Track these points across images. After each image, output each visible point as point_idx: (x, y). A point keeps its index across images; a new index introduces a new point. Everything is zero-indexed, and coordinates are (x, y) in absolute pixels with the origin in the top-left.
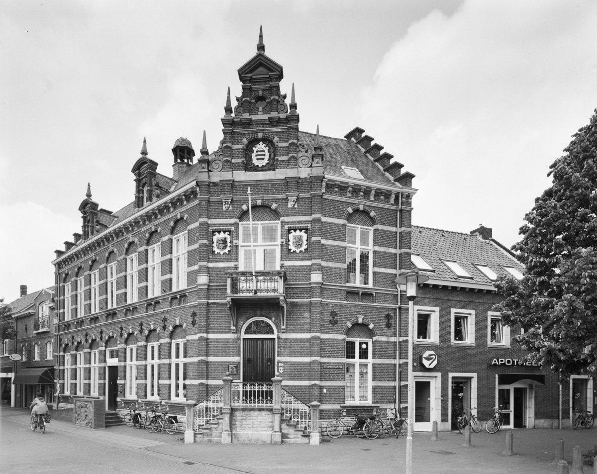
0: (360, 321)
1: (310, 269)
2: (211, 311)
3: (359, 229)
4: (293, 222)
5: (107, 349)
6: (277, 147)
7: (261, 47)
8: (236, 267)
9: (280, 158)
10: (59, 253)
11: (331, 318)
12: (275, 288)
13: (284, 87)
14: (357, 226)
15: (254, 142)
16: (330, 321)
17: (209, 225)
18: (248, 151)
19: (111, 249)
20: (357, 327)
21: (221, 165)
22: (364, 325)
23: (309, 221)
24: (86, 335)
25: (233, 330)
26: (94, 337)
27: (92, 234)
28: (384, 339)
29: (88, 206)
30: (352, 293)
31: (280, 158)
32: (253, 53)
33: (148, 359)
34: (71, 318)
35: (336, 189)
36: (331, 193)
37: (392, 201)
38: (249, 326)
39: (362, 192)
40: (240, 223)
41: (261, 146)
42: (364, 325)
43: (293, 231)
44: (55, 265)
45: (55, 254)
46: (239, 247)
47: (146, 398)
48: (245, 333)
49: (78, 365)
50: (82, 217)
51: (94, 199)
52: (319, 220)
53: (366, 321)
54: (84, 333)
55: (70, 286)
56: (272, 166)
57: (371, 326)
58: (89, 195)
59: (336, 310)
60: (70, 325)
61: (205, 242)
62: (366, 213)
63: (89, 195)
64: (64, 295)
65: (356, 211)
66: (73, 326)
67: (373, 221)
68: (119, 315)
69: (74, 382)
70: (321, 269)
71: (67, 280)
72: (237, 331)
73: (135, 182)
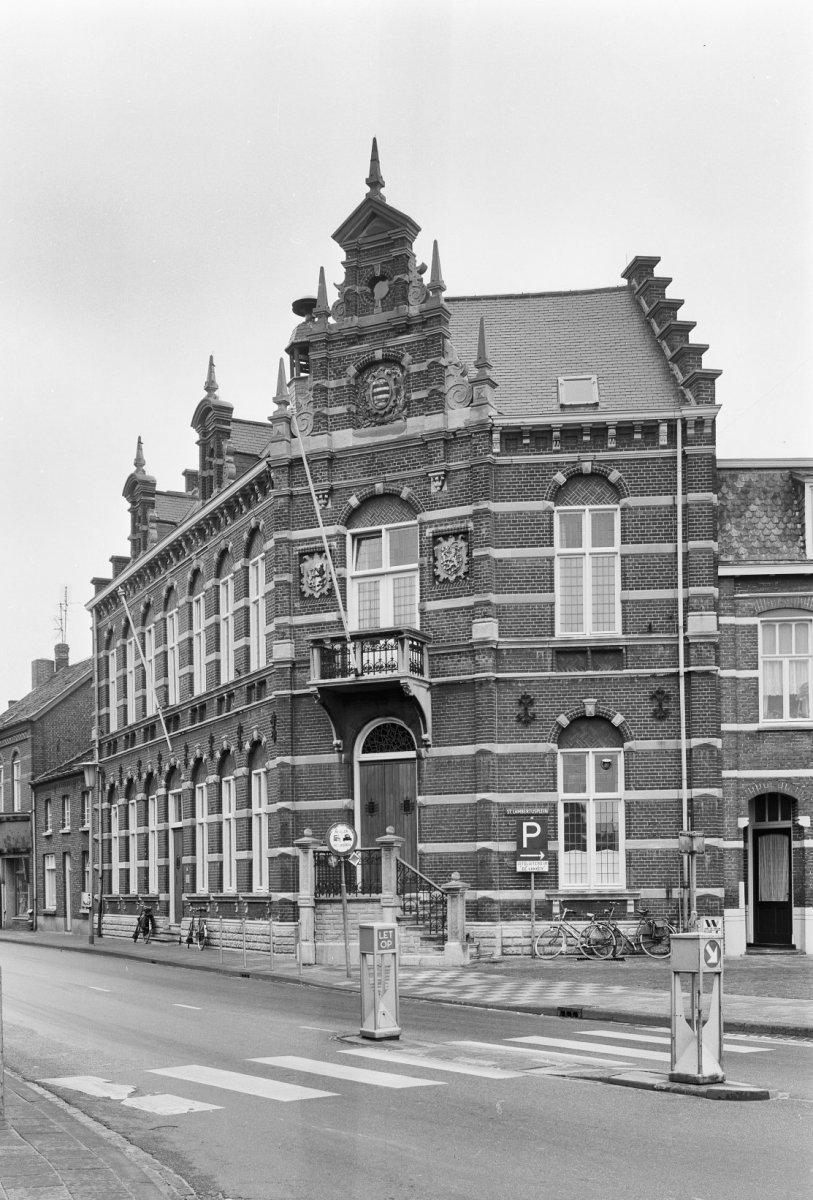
0: (590, 710)
1: (471, 612)
2: (300, 715)
3: (587, 513)
4: (440, 521)
5: (171, 792)
7: (375, 182)
8: (340, 624)
9: (414, 396)
10: (100, 584)
11: (520, 711)
12: (392, 663)
13: (421, 251)
14: (581, 507)
17: (290, 543)
18: (355, 391)
20: (583, 726)
21: (311, 421)
22: (602, 719)
23: (470, 516)
25: (338, 746)
27: (220, 483)
28: (652, 745)
30: (567, 652)
33: (223, 811)
36: (515, 449)
37: (663, 441)
38: (369, 739)
39: (586, 435)
42: (602, 719)
43: (441, 539)
44: (91, 611)
45: (93, 587)
46: (349, 581)
47: (222, 891)
48: (364, 752)
49: (255, 809)
50: (197, 443)
51: (223, 396)
52: (487, 512)
53: (604, 709)
54: (235, 724)
55: (231, 585)
57: (618, 720)
58: (211, 387)
59: (532, 692)
62: (599, 476)
63: (211, 387)
64: (108, 677)
66: (240, 697)
67: (617, 491)
69: (244, 855)
71: (225, 567)
72: (348, 748)
73: (197, 448)
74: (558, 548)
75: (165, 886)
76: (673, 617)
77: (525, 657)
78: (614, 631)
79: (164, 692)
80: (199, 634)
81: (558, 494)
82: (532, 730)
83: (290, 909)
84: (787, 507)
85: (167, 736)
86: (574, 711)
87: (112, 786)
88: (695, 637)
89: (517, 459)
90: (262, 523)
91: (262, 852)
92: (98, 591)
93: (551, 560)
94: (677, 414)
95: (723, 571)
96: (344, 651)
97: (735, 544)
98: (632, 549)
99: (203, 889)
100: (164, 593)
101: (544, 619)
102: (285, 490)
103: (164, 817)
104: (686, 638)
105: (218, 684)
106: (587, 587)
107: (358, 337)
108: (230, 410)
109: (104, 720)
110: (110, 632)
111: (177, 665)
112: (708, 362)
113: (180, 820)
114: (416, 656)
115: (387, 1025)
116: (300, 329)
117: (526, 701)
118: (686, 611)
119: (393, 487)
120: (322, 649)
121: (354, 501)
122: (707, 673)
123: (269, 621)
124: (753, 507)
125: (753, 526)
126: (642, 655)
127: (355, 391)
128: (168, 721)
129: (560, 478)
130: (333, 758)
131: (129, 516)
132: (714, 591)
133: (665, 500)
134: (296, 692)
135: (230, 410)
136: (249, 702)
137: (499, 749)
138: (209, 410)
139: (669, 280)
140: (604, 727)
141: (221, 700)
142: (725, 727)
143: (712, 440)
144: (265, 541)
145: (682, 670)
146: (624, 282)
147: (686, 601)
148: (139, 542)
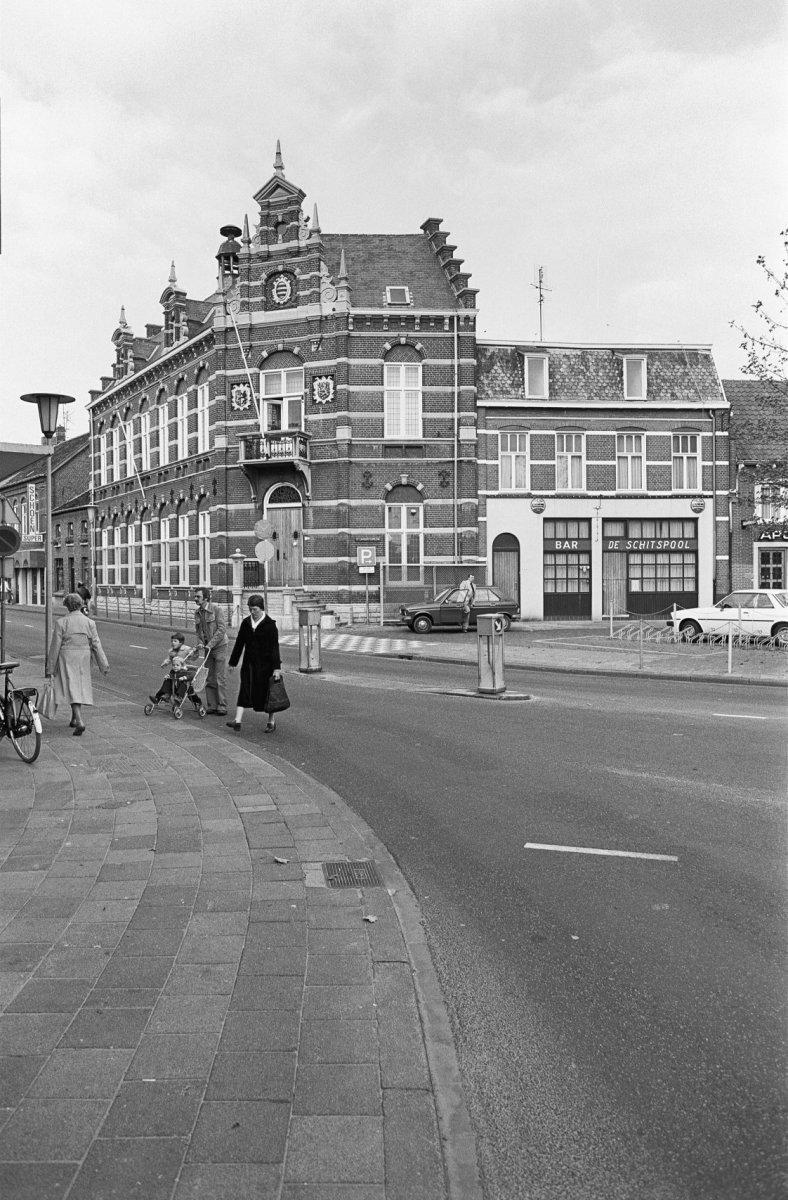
0: (404, 481)
1: (337, 422)
6: (298, 281)
9: (301, 293)
12: (286, 451)
13: (307, 208)
15: (274, 275)
16: (363, 484)
18: (267, 289)
19: (161, 386)
20: (400, 490)
24: (122, 505)
26: (202, 490)
28: (439, 502)
29: (122, 336)
31: (301, 293)
32: (271, 173)
34: (152, 466)
35: (368, 324)
37: (447, 328)
40: (261, 372)
41: (282, 279)
56: (294, 302)
57: (420, 487)
60: (118, 487)
61: (222, 397)
65: (396, 345)
68: (152, 479)
70: (348, 422)
71: (182, 388)
72: (259, 500)
74: (386, 386)
75: (139, 581)
76: (452, 428)
77: (367, 450)
78: (416, 435)
79: (139, 462)
80: (163, 428)
81: (386, 356)
82: (373, 492)
83: (225, 596)
84: (515, 367)
85: (142, 489)
86: (394, 481)
87: (103, 518)
88: (464, 440)
89: (363, 334)
90: (207, 365)
91: (206, 562)
92: (93, 400)
93: (382, 393)
94: (455, 313)
95: (479, 403)
96: (258, 444)
97: (486, 388)
98: (429, 389)
99: (165, 583)
100: (140, 402)
101: (378, 428)
102: (223, 346)
103: (139, 538)
104: (459, 441)
105: (177, 459)
106: (403, 404)
107: (268, 256)
108: (185, 294)
109: (97, 477)
110: (102, 423)
111: (149, 445)
112: (472, 284)
113: (149, 540)
114: (302, 447)
115: (315, 665)
116: (224, 245)
117: (367, 475)
118: (459, 426)
119: (288, 347)
120: (246, 441)
121: (265, 354)
122: (469, 462)
123: (211, 423)
124: (495, 367)
125: (495, 378)
126: (434, 450)
127: (267, 289)
128: (142, 480)
129: (388, 346)
130: (251, 506)
131: (115, 353)
132: (474, 414)
133: (448, 362)
134: (229, 466)
135: (185, 294)
136: (197, 471)
137: (354, 503)
138: (171, 294)
139: (448, 234)
140: (411, 490)
141: (179, 469)
142: (480, 492)
143: (473, 329)
144: (209, 376)
145: (456, 459)
146: (422, 232)
147: (459, 420)
148: (120, 372)
